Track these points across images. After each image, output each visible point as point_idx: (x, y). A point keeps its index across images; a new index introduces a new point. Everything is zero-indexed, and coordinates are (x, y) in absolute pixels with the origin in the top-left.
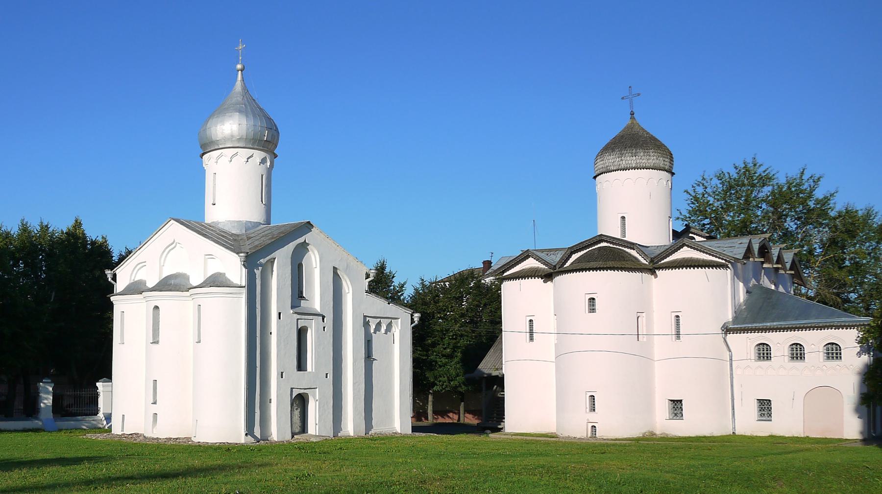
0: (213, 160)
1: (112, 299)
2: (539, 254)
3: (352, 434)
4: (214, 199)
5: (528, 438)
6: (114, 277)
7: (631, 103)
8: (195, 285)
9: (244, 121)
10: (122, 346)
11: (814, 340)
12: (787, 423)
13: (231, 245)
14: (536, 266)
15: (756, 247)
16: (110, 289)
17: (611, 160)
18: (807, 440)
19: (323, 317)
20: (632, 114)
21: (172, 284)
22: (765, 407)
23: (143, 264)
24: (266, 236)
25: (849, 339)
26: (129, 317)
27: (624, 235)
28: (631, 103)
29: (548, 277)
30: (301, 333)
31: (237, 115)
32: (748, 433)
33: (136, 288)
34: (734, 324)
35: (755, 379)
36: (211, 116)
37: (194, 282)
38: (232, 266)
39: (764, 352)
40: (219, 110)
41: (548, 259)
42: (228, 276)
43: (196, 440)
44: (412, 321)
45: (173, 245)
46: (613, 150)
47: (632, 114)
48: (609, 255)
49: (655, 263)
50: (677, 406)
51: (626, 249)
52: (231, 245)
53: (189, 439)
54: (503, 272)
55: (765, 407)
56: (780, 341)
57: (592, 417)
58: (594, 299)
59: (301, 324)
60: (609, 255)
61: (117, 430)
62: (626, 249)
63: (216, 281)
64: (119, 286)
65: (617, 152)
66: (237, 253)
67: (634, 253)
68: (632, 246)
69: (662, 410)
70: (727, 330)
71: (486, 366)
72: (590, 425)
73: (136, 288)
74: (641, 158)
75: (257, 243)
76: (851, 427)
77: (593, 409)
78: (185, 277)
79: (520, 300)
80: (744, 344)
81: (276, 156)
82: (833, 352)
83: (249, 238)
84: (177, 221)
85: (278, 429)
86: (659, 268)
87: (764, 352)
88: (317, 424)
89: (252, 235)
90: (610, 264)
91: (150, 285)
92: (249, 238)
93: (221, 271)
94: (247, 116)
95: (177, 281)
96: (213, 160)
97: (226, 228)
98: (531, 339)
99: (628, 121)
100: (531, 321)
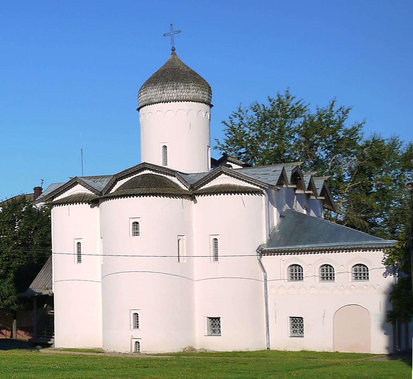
2: (86, 181)
11: (343, 261)
12: (318, 339)
17: (153, 93)
18: (336, 355)
20: (173, 50)
22: (297, 324)
25: (375, 260)
29: (95, 202)
32: (282, 349)
35: (289, 298)
39: (296, 273)
41: (95, 185)
47: (173, 50)
48: (152, 182)
49: (194, 189)
50: (215, 323)
51: (168, 177)
54: (53, 198)
55: (297, 324)
56: (311, 263)
57: (136, 333)
58: (137, 223)
60: (152, 182)
65: (159, 85)
67: (175, 180)
68: (173, 173)
69: (201, 327)
70: (262, 252)
71: (37, 286)
72: (134, 341)
74: (182, 91)
76: (378, 343)
77: (137, 326)
79: (69, 225)
82: (361, 272)
86: (198, 194)
87: (296, 273)
98: (79, 260)
99: (169, 57)
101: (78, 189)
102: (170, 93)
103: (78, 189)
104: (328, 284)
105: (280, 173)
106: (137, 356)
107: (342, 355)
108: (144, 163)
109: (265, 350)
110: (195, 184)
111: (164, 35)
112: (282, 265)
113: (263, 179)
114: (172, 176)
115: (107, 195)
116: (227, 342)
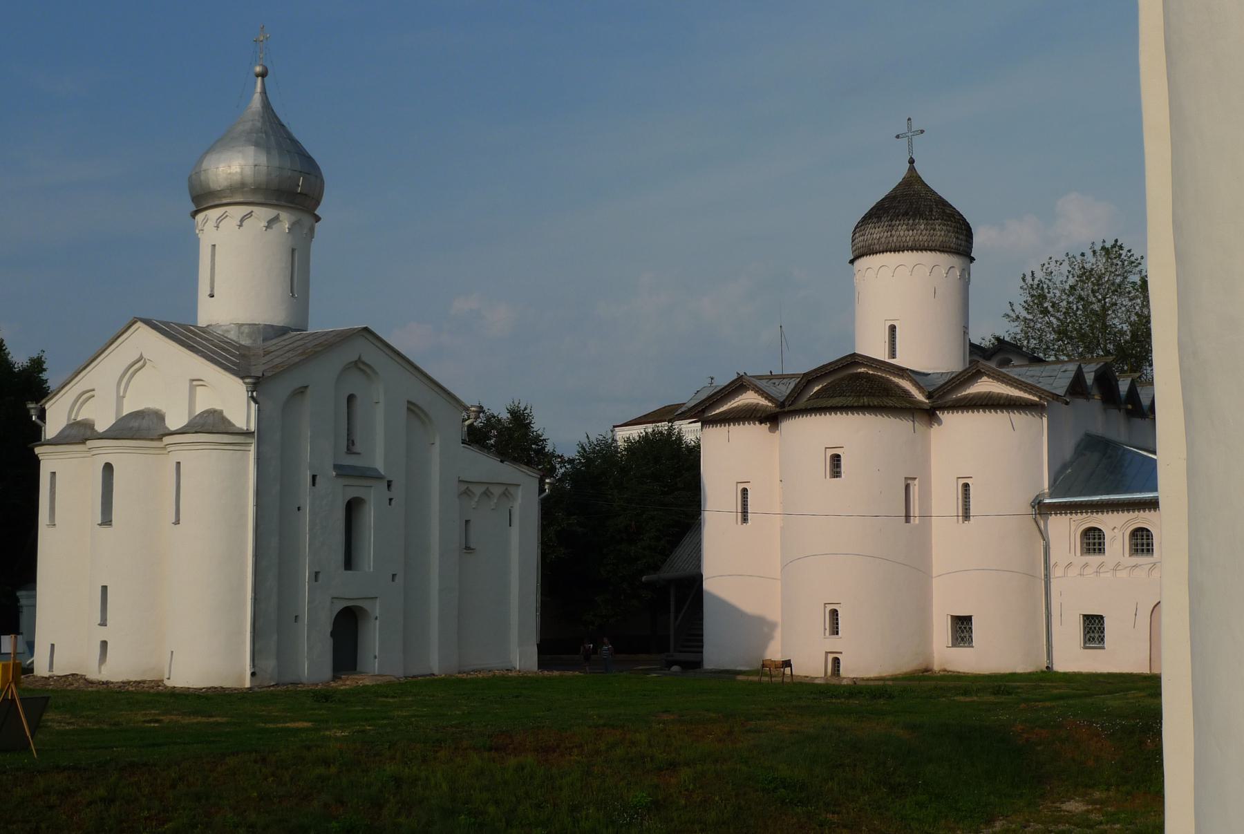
0: (210, 225)
1: (37, 450)
2: (758, 383)
3: (436, 671)
4: (212, 288)
5: (751, 678)
6: (42, 415)
7: (910, 144)
8: (173, 428)
9: (263, 159)
10: (52, 529)
13: (234, 363)
14: (756, 401)
15: (1089, 378)
16: (34, 433)
17: (876, 233)
19: (389, 484)
20: (912, 161)
21: (141, 428)
22: (1093, 627)
23: (88, 395)
24: (293, 350)
26: (66, 480)
27: (893, 355)
28: (910, 144)
29: (772, 418)
30: (353, 508)
31: (251, 150)
33: (79, 434)
34: (1051, 496)
36: (210, 150)
37: (101, 427)
38: (232, 398)
39: (1093, 541)
40: (222, 142)
41: (773, 391)
42: (228, 415)
43: (169, 684)
44: (542, 490)
45: (139, 363)
46: (879, 218)
47: (912, 161)
48: (856, 386)
49: (939, 399)
50: (962, 627)
51: (896, 380)
52: (234, 363)
53: (158, 683)
54: (945, 394)
55: (1093, 627)
57: (833, 644)
58: (839, 456)
59: (353, 493)
60: (856, 386)
61: (41, 668)
62: (896, 380)
63: (210, 424)
64: (53, 425)
65: (885, 222)
66: (242, 378)
67: (906, 384)
68: (902, 372)
69: (941, 631)
70: (1041, 509)
71: (675, 568)
72: (830, 657)
73: (79, 434)
74: (921, 231)
75: (278, 361)
77: (835, 630)
78: (159, 417)
79: (729, 458)
80: (1064, 530)
81: (318, 219)
83: (267, 353)
84: (148, 322)
85: (311, 662)
86: (944, 408)
87: (1093, 541)
88: (380, 658)
89: (274, 348)
90: (850, 401)
91: (101, 427)
92: (267, 353)
93: (218, 408)
94: (268, 152)
95: (145, 423)
96: (210, 225)
97: (232, 335)
98: (745, 520)
99: (901, 172)
100: (966, 486)
101: (749, 398)
102: (902, 232)
103: (749, 398)
104: (1094, 559)
105: (1072, 374)
106: (834, 681)
107: (891, 697)
108: (854, 354)
109: (1042, 672)
110: (935, 391)
111: (922, 132)
112: (1073, 528)
113: (1044, 385)
114: (902, 377)
115: (792, 408)
116: (989, 656)
